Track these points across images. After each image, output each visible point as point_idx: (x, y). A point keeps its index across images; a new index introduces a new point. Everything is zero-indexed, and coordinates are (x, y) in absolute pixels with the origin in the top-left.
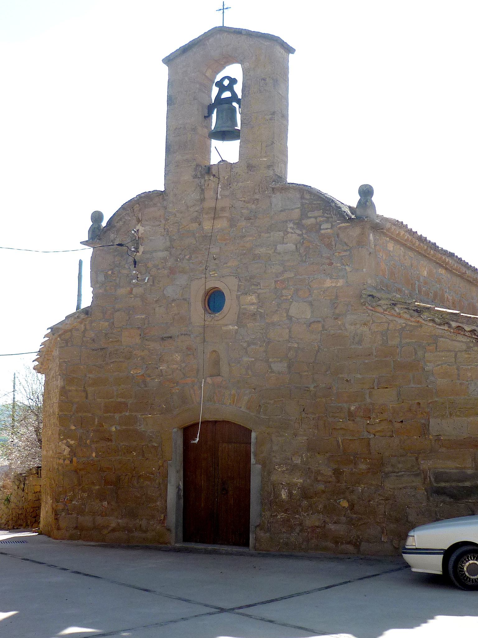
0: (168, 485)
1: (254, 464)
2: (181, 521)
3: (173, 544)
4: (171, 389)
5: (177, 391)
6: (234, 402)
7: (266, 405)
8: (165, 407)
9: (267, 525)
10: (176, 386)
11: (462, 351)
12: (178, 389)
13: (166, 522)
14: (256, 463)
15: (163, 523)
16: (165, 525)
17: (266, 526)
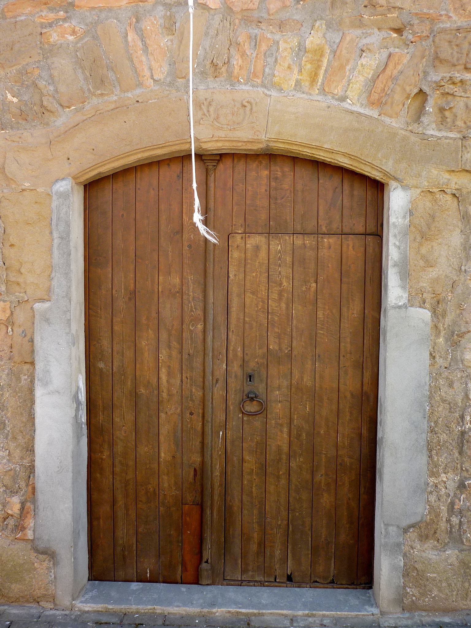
0: (39, 392)
1: (400, 307)
2: (336, 165)
3: (66, 601)
4: (44, 31)
5: (71, 38)
6: (313, 80)
7: (449, 88)
8: (15, 100)
9: (448, 521)
10: (65, 20)
11: (203, 456)
12: (74, 32)
13: (30, 522)
14: (411, 303)
15: (20, 527)
16: (30, 534)
17: (443, 525)
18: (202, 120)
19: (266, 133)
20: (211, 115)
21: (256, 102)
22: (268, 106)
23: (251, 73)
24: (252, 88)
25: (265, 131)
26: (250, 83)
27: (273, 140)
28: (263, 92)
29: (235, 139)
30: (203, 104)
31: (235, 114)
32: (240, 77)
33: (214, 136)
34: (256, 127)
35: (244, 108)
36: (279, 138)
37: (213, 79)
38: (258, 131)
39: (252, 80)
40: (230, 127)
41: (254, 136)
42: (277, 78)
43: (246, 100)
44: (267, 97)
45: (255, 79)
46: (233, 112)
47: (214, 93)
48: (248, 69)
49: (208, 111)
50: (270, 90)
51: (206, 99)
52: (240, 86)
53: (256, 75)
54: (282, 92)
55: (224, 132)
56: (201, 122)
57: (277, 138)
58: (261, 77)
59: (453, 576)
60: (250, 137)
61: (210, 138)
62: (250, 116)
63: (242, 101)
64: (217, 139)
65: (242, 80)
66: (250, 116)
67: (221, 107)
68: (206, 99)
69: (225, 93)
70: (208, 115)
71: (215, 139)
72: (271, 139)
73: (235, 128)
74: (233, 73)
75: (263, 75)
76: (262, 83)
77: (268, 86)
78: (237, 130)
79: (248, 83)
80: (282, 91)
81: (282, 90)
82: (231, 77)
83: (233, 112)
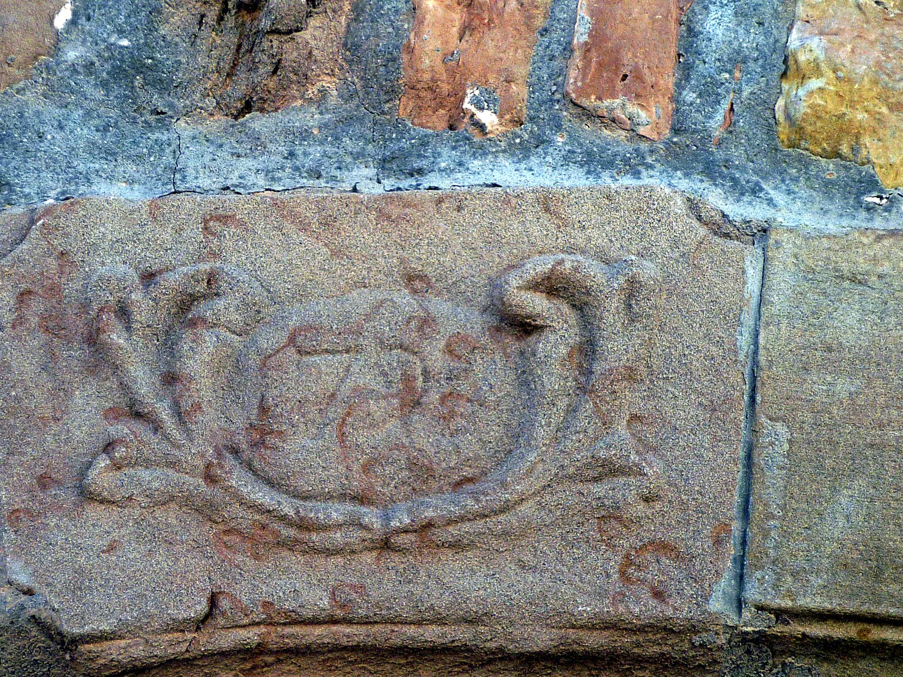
18: (103, 462)
19: (740, 561)
20: (198, 407)
21: (632, 282)
22: (748, 319)
23: (568, 49)
24: (581, 172)
25: (732, 549)
26: (559, 140)
27: (817, 630)
28: (694, 206)
29: (431, 634)
30: (123, 312)
31: (434, 397)
32: (471, 93)
33: (224, 604)
34: (641, 508)
35: (513, 345)
36: (882, 609)
37: (221, 120)
38: (663, 547)
39: (589, 115)
40: (387, 518)
41: (619, 597)
42: (814, 83)
43: (539, 266)
44: (733, 245)
45: (615, 104)
46: (408, 379)
47: (224, 219)
48: (540, 22)
49: (170, 379)
50: (756, 190)
51: (149, 278)
52: (475, 164)
53: (617, 63)
54: (869, 209)
55: (320, 561)
56: (92, 474)
57: (851, 607)
58: (668, 81)
59: (702, 114)
60: (585, 608)
61: (179, 626)
62: (572, 410)
63: (495, 285)
64: (251, 636)
65: (487, 118)
66: (572, 410)
67: (292, 340)
68: (149, 278)
69: (328, 223)
70: (164, 413)
71: (227, 640)
72: (797, 628)
73: (429, 525)
74: (405, 58)
75: (686, 70)
76: (676, 131)
77: (737, 154)
78: (457, 546)
79: (541, 141)
80: (871, 199)
81: (872, 184)
82: (392, 93)
83: (408, 379)
